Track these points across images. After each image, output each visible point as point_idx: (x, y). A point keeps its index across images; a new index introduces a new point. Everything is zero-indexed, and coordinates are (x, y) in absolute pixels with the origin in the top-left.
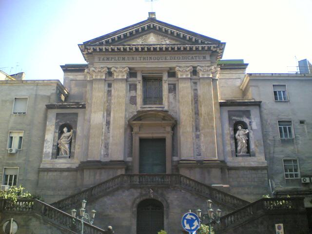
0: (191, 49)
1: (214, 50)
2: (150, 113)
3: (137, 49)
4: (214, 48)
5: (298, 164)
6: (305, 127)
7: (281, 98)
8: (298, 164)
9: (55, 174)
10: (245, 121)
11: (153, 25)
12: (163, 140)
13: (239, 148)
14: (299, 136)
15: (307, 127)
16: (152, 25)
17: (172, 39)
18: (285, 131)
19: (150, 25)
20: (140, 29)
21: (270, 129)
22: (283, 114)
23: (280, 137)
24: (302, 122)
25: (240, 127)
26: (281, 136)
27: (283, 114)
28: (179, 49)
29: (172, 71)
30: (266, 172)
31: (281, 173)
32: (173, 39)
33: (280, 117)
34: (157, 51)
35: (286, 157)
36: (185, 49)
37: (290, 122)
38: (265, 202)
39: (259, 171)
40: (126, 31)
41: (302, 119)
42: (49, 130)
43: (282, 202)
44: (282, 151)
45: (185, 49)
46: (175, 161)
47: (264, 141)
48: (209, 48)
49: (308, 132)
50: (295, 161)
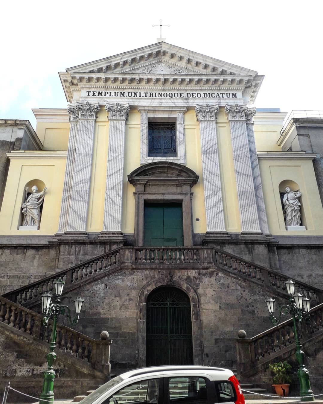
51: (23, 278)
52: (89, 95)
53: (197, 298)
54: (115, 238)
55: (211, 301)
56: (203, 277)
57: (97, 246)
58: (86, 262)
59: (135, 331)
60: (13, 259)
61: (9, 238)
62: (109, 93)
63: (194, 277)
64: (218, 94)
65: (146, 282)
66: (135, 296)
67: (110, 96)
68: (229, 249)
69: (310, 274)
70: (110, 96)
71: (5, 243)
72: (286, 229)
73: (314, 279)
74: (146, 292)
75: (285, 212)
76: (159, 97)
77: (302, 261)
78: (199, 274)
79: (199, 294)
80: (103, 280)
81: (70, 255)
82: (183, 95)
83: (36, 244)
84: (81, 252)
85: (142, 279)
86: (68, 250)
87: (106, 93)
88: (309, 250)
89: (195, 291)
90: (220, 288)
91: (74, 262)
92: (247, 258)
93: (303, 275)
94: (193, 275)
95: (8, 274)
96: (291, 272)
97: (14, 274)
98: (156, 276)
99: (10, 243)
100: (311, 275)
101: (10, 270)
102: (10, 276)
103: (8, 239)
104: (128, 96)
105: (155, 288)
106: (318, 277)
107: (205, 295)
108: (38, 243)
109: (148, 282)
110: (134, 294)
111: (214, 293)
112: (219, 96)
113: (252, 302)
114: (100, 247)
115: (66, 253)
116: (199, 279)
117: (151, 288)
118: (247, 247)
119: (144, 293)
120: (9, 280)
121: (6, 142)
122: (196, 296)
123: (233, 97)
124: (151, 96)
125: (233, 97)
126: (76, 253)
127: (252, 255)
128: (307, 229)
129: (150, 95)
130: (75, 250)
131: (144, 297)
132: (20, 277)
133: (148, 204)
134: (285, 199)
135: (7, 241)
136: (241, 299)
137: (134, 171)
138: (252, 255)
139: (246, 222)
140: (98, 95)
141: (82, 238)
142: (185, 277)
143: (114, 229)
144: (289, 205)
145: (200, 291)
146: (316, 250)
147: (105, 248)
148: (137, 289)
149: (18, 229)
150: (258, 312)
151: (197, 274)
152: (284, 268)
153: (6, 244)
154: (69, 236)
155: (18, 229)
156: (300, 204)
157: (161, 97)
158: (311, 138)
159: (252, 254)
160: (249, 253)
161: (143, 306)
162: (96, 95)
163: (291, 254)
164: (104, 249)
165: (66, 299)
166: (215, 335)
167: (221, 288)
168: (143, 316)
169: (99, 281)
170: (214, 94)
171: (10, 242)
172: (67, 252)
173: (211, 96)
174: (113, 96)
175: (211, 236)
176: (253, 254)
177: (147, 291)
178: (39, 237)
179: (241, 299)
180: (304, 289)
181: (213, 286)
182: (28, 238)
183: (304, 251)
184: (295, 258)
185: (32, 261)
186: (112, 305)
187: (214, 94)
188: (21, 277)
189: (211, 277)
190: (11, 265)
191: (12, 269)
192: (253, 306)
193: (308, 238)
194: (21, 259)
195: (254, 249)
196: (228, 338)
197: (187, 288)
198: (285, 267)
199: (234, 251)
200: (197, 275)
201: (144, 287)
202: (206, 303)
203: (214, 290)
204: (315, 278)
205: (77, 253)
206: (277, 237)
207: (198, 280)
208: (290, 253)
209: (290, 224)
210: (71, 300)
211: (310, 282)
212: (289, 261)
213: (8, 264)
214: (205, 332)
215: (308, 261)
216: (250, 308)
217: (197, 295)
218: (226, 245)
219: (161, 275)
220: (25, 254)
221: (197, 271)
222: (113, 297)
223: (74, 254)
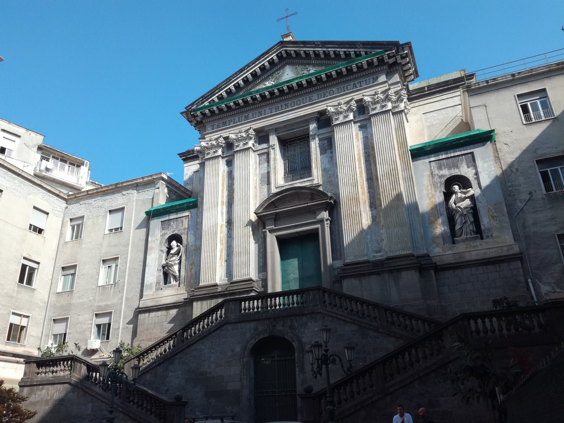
0: (350, 71)
1: (391, 61)
2: (303, 191)
3: (263, 97)
4: (390, 57)
5: (559, 244)
7: (538, 116)
9: (159, 313)
10: (463, 174)
11: (286, 51)
12: (313, 236)
13: (458, 227)
17: (318, 65)
19: (281, 52)
20: (267, 64)
21: (521, 180)
23: (544, 192)
25: (456, 188)
28: (329, 76)
29: (323, 118)
30: (519, 263)
32: (321, 65)
34: (364, 70)
36: (339, 74)
38: (472, 322)
39: (505, 266)
40: (236, 80)
42: (152, 248)
45: (339, 74)
46: (338, 268)
47: (507, 206)
48: (381, 61)
62: (233, 120)
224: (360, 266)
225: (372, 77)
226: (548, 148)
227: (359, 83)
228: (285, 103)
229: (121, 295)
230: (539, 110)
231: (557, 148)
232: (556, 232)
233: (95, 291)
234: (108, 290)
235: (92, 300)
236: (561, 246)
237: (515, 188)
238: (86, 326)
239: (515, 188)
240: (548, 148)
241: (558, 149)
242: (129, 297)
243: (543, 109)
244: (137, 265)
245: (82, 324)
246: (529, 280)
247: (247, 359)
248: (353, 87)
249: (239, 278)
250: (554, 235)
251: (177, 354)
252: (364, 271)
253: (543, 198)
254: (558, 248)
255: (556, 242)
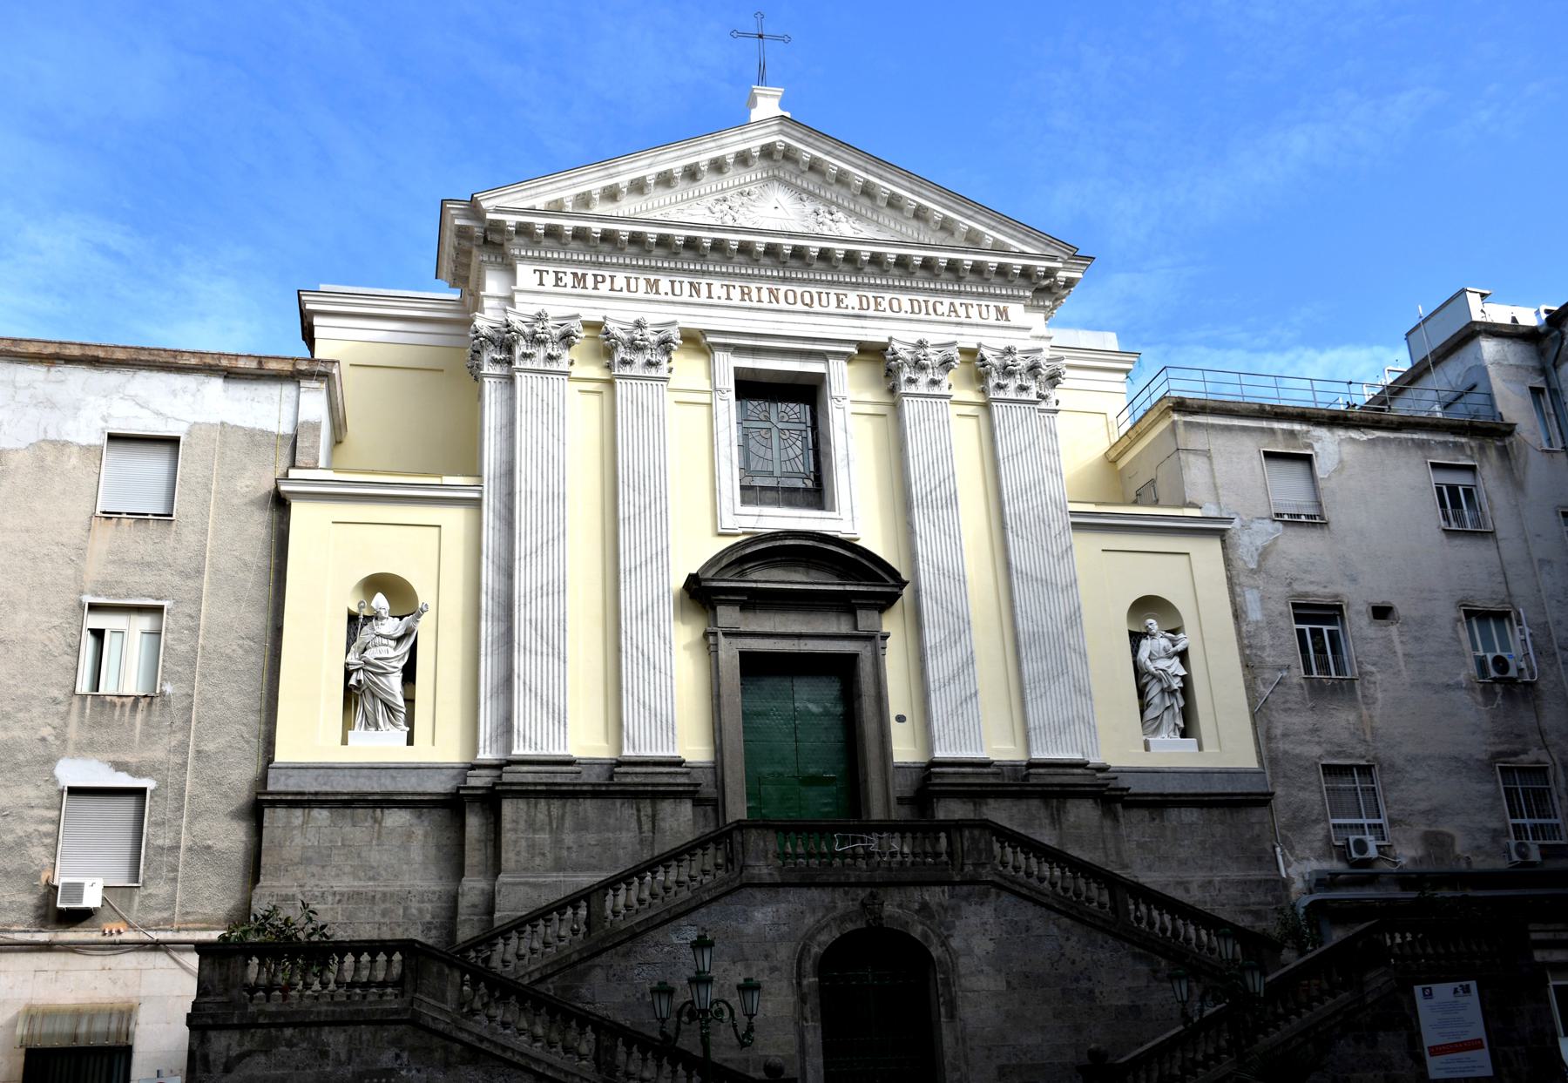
5: (1502, 787)
6: (1394, 630)
8: (1324, 786)
14: (1373, 669)
15: (1401, 634)
16: (304, 339)
18: (1320, 650)
22: (1308, 577)
24: (1382, 613)
26: (1308, 670)
27: (1308, 577)
31: (1316, 821)
33: (1299, 587)
35: (1330, 754)
37: (1340, 608)
41: (1379, 600)
43: (1403, 938)
44: (1315, 731)
49: (1405, 655)
50: (1365, 771)
51: (384, 901)
52: (541, 284)
53: (949, 960)
54: (665, 780)
55: (985, 968)
56: (963, 904)
57: (614, 804)
58: (642, 866)
59: (793, 1052)
60: (343, 840)
61: (322, 771)
62: (608, 280)
63: (940, 905)
64: (952, 304)
65: (812, 920)
66: (785, 958)
67: (612, 290)
68: (999, 813)
69: (1207, 879)
70: (612, 290)
71: (312, 790)
72: (1147, 747)
73: (1217, 892)
74: (816, 950)
75: (1142, 693)
76: (771, 302)
77: (1186, 842)
78: (951, 897)
79: (954, 951)
80: (694, 915)
81: (535, 831)
82: (846, 301)
83: (413, 794)
84: (568, 823)
85: (802, 913)
86: (527, 813)
87: (600, 279)
88: (1205, 810)
89: (943, 944)
90: (1007, 932)
91: (548, 854)
92: (1047, 837)
93: (1187, 882)
94: (937, 900)
95: (335, 889)
96: (1156, 874)
97: (351, 886)
98: (839, 904)
99: (328, 789)
100: (1210, 882)
101: (338, 875)
102: (342, 894)
103: (319, 776)
104: (670, 293)
105: (838, 935)
106: (1227, 888)
107: (969, 952)
108: (420, 790)
109: (818, 921)
110: (784, 953)
111: (990, 946)
112: (955, 311)
113: (1086, 969)
114: (623, 804)
115: (522, 825)
116: (953, 909)
117: (826, 938)
118: (1047, 805)
119: (809, 950)
120: (339, 908)
121: (265, 433)
122: (948, 956)
123: (997, 319)
124: (746, 297)
125: (997, 319)
126: (551, 823)
127: (1061, 828)
128: (1200, 748)
129: (743, 292)
130: (549, 815)
131: (811, 962)
132: (374, 897)
133: (754, 666)
134: (1143, 654)
135: (316, 780)
136: (1059, 960)
137: (711, 560)
138: (1061, 828)
139: (1035, 729)
140: (574, 287)
141: (566, 778)
142: (916, 906)
143: (659, 749)
144: (1154, 676)
145: (955, 943)
146: (1221, 810)
147: (638, 810)
148: (790, 941)
149: (345, 742)
150: (1101, 993)
151: (946, 895)
152: (1139, 861)
153: (316, 794)
154: (525, 768)
155: (345, 742)
156: (1183, 672)
157: (778, 302)
158: (1215, 461)
159: (1060, 823)
160: (1053, 822)
161: (809, 985)
162: (565, 286)
163: (1157, 822)
164: (635, 812)
165: (599, 970)
166: (998, 1057)
167: (1010, 934)
168: (812, 1012)
169: (683, 921)
170: (942, 303)
171: (325, 784)
172: (526, 821)
173: (931, 310)
174: (621, 290)
175: (948, 774)
176: (1064, 826)
177: (819, 946)
178: (417, 768)
179: (1059, 960)
180: (1031, 855)
181: (988, 927)
182: (383, 771)
183: (1191, 815)
184: (1168, 833)
185: (405, 847)
186: (726, 986)
187: (942, 303)
188: (378, 896)
189: (982, 904)
190: (337, 859)
191: (344, 874)
192: (1090, 980)
193: (1205, 773)
194: (368, 839)
195: (1064, 812)
196: (1030, 1062)
197: (925, 935)
198: (1142, 860)
199: (1011, 818)
200: (946, 899)
201: (810, 937)
202: (972, 974)
203: (991, 939)
204: (1220, 890)
205: (555, 826)
206: (1122, 771)
207: (950, 913)
208: (1154, 819)
209: (1156, 731)
210: (611, 972)
211: (1205, 902)
212: (1151, 842)
213: (329, 856)
214: (972, 1049)
215: (1202, 843)
216: (1084, 985)
217: (950, 954)
218: (991, 801)
219: (853, 900)
220: (380, 824)
221: (946, 888)
222: (726, 964)
223: (548, 828)
224: (644, 769)
225: (997, 304)
226: (1312, 583)
227: (538, 273)
228: (691, 280)
229: (179, 736)
230: (1462, 508)
231: (1325, 587)
232: (1319, 758)
233: (62, 708)
234: (122, 714)
235: (51, 739)
236: (1505, 789)
237: (1254, 651)
238: (31, 828)
239: (1254, 651)
240: (1312, 583)
241: (1327, 590)
242: (210, 747)
243: (1452, 507)
244: (235, 647)
245: (9, 819)
246: (1278, 849)
247: (812, 980)
248: (950, 311)
249: (545, 752)
250: (1316, 764)
251: (598, 954)
252: (678, 785)
253: (1301, 686)
254: (1321, 792)
255: (1319, 780)
